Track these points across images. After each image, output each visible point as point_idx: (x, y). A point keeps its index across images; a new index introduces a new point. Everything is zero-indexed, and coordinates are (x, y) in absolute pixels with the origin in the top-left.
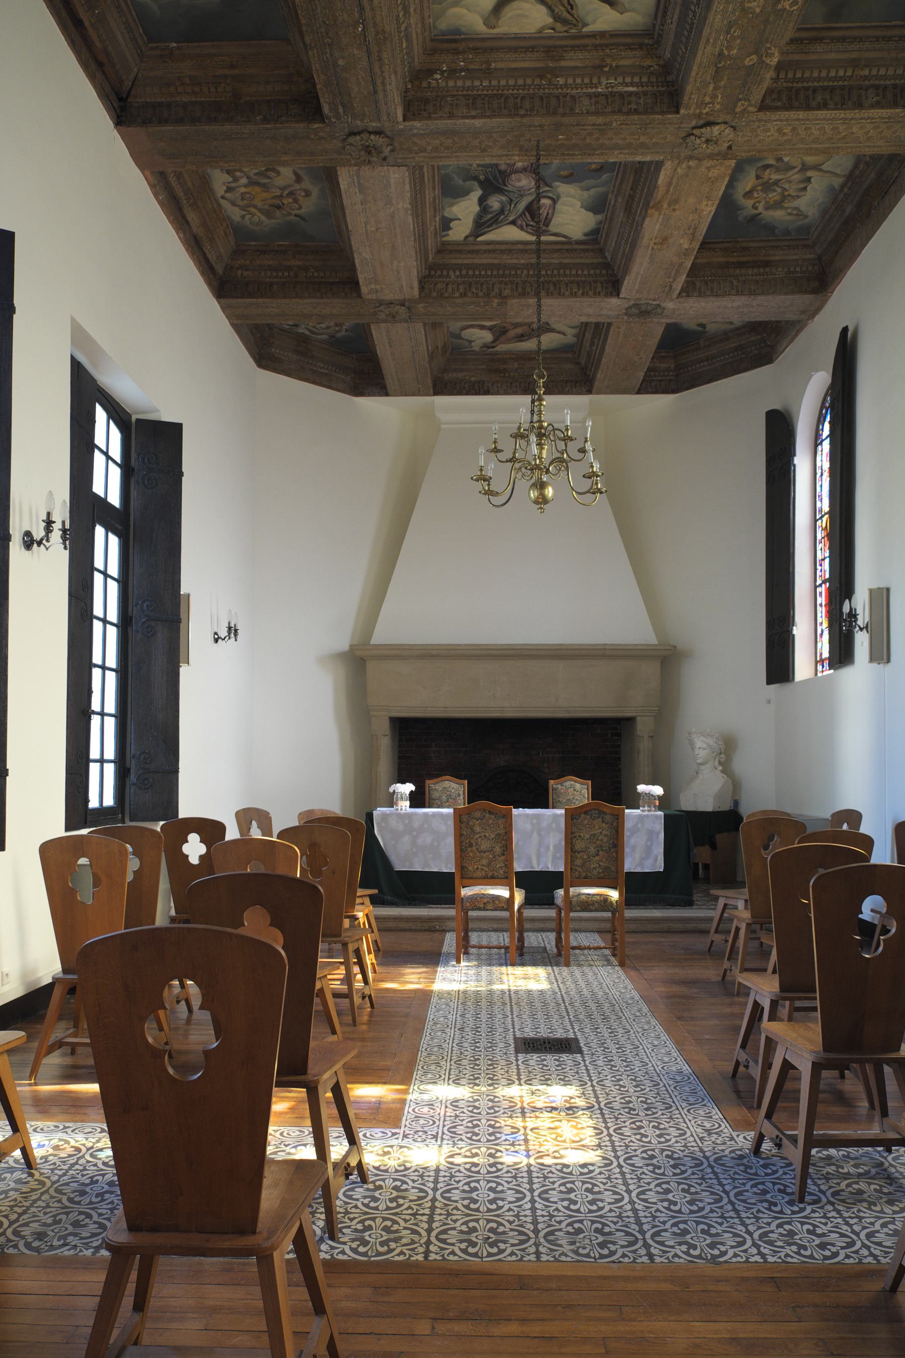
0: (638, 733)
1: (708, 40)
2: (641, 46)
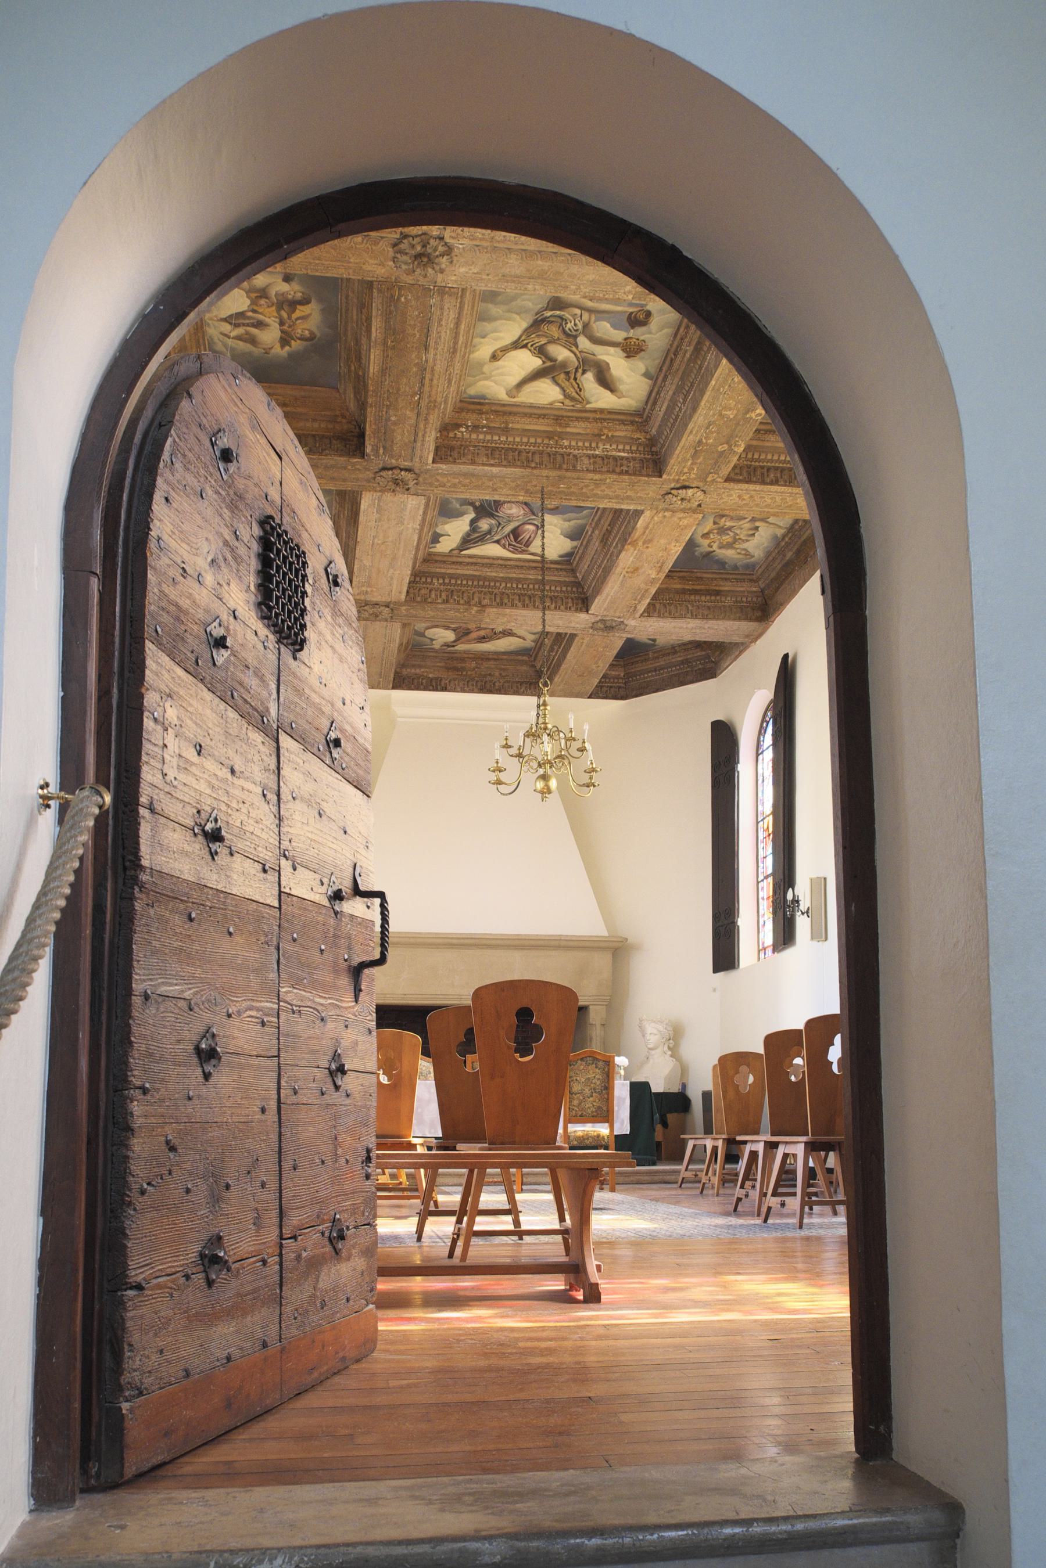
0: (591, 1021)
1: (691, 432)
2: (632, 423)
